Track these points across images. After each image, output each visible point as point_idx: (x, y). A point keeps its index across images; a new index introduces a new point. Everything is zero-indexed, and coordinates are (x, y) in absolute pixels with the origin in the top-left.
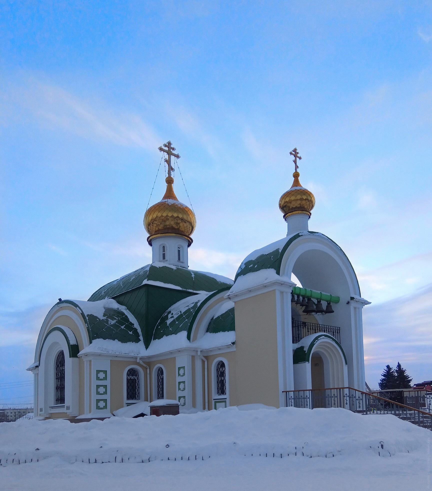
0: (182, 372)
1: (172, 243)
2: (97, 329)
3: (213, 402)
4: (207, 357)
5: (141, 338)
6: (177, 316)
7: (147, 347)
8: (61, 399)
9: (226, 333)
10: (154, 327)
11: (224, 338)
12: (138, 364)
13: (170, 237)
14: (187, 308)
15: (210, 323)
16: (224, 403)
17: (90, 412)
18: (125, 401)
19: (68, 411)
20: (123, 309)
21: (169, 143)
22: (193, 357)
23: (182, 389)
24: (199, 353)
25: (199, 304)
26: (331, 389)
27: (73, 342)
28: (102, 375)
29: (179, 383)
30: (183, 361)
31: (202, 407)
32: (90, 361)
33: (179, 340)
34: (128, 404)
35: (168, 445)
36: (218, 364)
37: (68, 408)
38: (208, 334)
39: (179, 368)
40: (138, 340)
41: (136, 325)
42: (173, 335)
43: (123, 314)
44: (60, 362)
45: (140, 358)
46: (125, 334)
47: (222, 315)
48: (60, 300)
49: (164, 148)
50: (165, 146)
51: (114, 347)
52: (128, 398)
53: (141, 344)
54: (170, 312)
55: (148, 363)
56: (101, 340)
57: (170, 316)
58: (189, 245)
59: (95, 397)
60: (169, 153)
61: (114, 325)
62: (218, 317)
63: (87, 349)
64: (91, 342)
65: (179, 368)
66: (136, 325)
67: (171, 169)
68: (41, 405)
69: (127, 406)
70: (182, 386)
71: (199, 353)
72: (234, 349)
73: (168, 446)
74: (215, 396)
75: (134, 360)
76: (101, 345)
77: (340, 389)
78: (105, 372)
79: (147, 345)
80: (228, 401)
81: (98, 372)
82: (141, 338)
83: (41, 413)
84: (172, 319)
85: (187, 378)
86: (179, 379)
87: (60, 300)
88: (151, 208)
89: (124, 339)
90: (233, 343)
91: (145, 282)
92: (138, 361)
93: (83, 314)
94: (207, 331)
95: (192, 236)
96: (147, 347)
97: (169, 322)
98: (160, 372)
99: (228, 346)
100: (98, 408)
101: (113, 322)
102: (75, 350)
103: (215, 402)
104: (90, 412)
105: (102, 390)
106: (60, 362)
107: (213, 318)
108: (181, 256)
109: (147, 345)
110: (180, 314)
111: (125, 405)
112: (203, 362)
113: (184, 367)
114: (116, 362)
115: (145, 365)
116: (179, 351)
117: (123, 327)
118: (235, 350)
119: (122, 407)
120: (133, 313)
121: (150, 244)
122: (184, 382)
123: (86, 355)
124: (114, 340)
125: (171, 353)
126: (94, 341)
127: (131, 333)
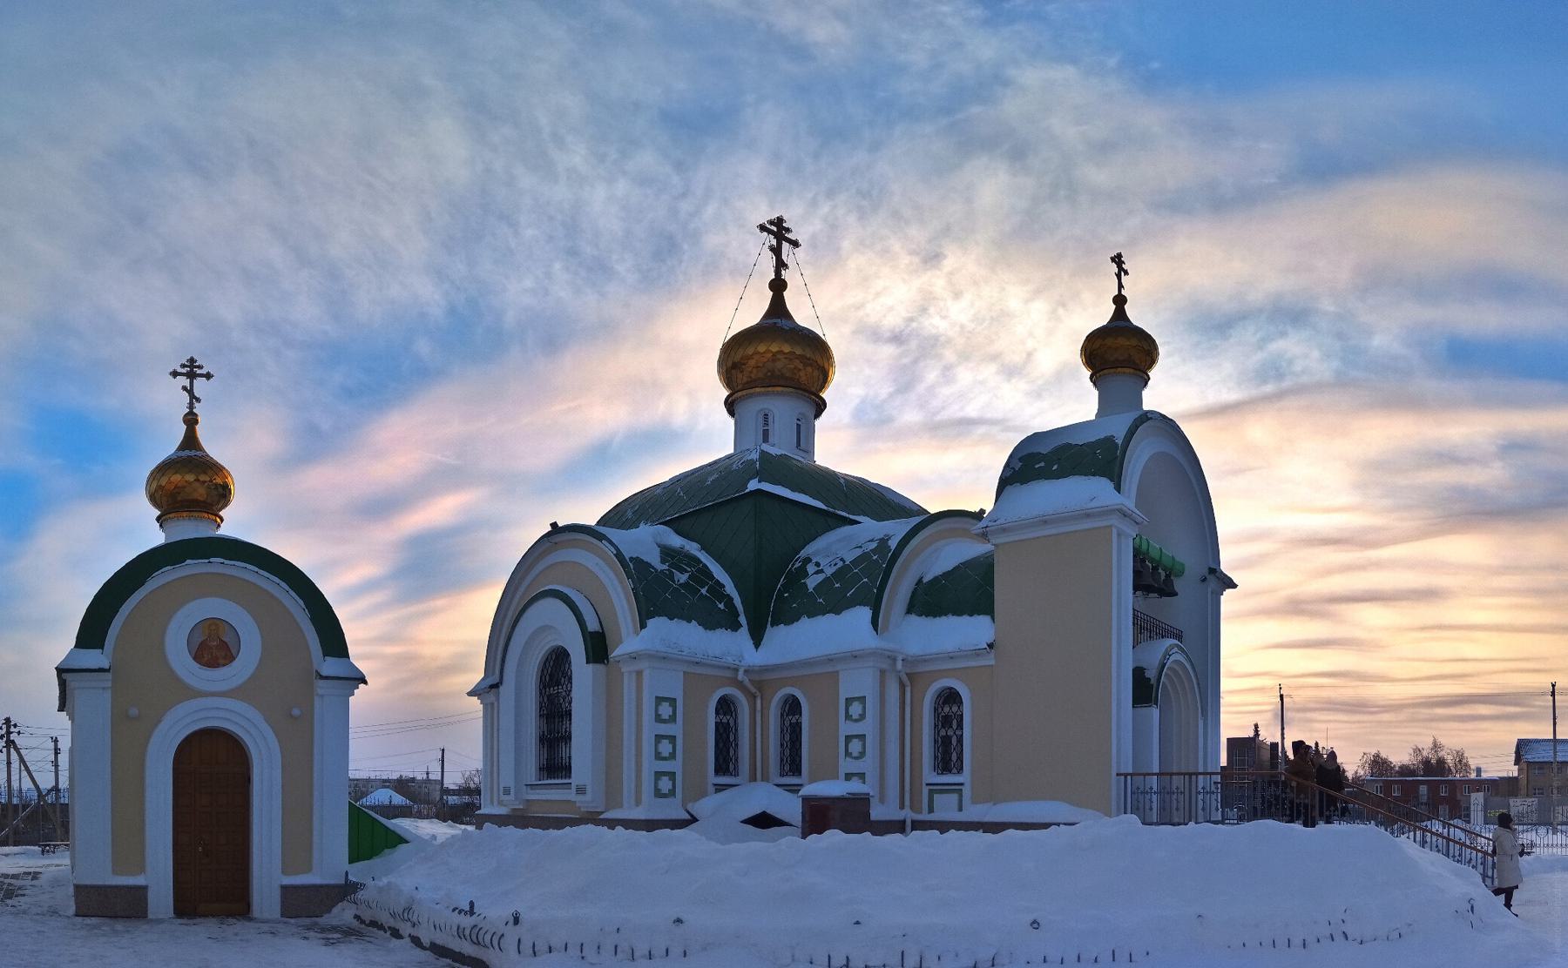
0: (855, 709)
1: (782, 409)
2: (657, 593)
3: (925, 790)
4: (911, 676)
5: (742, 619)
6: (834, 569)
7: (757, 645)
8: (555, 766)
9: (965, 619)
10: (773, 597)
11: (961, 633)
12: (740, 685)
13: (779, 394)
14: (858, 552)
15: (914, 593)
16: (955, 796)
17: (638, 802)
18: (712, 779)
19: (580, 798)
20: (693, 548)
21: (192, 360)
22: (883, 672)
23: (855, 754)
24: (899, 665)
25: (893, 544)
26: (1172, 774)
27: (592, 626)
28: (665, 710)
29: (848, 739)
30: (858, 682)
31: (633, 802)
32: (639, 673)
33: (849, 628)
34: (720, 788)
35: (1035, 922)
36: (786, 702)
37: (581, 790)
38: (913, 618)
39: (849, 701)
40: (735, 626)
41: (730, 588)
42: (830, 616)
43: (699, 561)
44: (556, 668)
45: (746, 671)
46: (712, 612)
47: (946, 575)
48: (554, 525)
49: (180, 370)
50: (183, 366)
51: (687, 636)
52: (718, 772)
53: (743, 636)
54: (808, 560)
55: (759, 682)
56: (664, 620)
57: (811, 569)
58: (818, 415)
59: (649, 766)
60: (192, 376)
61: (685, 585)
62: (936, 579)
63: (629, 641)
64: (643, 625)
65: (849, 701)
66: (730, 588)
67: (194, 398)
68: (507, 779)
69: (717, 791)
70: (855, 747)
71: (899, 665)
72: (990, 660)
73: (1035, 924)
74: (930, 776)
75: (728, 674)
76: (668, 632)
77: (1190, 775)
78: (672, 701)
79: (757, 639)
80: (966, 791)
81: (659, 700)
82: (742, 619)
83: (506, 798)
84: (821, 577)
85: (867, 727)
86: (846, 728)
87: (554, 525)
88: (734, 338)
89: (709, 624)
90: (991, 646)
91: (753, 485)
92: (741, 676)
93: (619, 555)
94: (909, 611)
95: (825, 395)
96: (757, 645)
97: (812, 582)
98: (792, 707)
99: (977, 653)
100: (658, 794)
101: (683, 578)
102: (598, 647)
103: (931, 793)
104: (902, 807)
105: (665, 748)
106: (556, 668)
107: (920, 581)
108: (804, 438)
109: (757, 639)
110: (840, 564)
111: (711, 789)
112: (902, 686)
113: (862, 699)
114: (696, 672)
115: (753, 690)
116: (855, 656)
117: (704, 591)
118: (993, 662)
119: (704, 794)
120: (718, 559)
121: (731, 412)
122: (862, 737)
123: (634, 657)
124: (689, 621)
125: (830, 660)
126: (651, 623)
127: (721, 606)
